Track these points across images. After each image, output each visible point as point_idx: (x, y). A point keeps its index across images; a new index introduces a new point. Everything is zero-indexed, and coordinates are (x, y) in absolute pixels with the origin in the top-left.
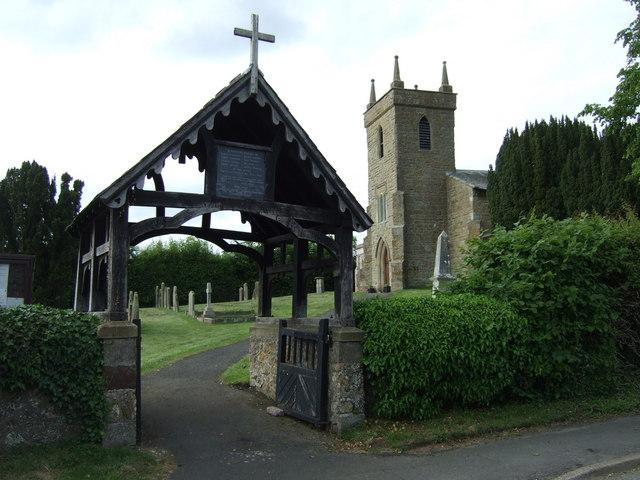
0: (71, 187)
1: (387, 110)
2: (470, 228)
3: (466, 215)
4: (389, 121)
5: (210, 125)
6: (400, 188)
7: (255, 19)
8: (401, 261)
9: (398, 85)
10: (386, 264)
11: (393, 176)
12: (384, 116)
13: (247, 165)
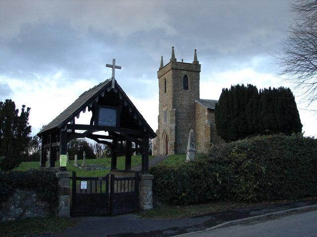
0: (26, 110)
1: (169, 71)
2: (206, 127)
3: (204, 121)
4: (169, 76)
5: (97, 100)
6: (174, 107)
7: (114, 60)
8: (173, 142)
9: (173, 60)
10: (167, 142)
11: (171, 103)
12: (167, 74)
13: (109, 116)
